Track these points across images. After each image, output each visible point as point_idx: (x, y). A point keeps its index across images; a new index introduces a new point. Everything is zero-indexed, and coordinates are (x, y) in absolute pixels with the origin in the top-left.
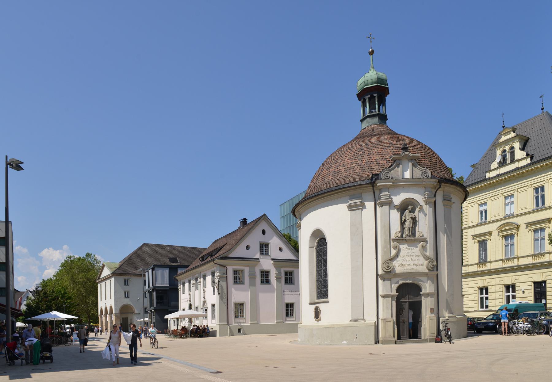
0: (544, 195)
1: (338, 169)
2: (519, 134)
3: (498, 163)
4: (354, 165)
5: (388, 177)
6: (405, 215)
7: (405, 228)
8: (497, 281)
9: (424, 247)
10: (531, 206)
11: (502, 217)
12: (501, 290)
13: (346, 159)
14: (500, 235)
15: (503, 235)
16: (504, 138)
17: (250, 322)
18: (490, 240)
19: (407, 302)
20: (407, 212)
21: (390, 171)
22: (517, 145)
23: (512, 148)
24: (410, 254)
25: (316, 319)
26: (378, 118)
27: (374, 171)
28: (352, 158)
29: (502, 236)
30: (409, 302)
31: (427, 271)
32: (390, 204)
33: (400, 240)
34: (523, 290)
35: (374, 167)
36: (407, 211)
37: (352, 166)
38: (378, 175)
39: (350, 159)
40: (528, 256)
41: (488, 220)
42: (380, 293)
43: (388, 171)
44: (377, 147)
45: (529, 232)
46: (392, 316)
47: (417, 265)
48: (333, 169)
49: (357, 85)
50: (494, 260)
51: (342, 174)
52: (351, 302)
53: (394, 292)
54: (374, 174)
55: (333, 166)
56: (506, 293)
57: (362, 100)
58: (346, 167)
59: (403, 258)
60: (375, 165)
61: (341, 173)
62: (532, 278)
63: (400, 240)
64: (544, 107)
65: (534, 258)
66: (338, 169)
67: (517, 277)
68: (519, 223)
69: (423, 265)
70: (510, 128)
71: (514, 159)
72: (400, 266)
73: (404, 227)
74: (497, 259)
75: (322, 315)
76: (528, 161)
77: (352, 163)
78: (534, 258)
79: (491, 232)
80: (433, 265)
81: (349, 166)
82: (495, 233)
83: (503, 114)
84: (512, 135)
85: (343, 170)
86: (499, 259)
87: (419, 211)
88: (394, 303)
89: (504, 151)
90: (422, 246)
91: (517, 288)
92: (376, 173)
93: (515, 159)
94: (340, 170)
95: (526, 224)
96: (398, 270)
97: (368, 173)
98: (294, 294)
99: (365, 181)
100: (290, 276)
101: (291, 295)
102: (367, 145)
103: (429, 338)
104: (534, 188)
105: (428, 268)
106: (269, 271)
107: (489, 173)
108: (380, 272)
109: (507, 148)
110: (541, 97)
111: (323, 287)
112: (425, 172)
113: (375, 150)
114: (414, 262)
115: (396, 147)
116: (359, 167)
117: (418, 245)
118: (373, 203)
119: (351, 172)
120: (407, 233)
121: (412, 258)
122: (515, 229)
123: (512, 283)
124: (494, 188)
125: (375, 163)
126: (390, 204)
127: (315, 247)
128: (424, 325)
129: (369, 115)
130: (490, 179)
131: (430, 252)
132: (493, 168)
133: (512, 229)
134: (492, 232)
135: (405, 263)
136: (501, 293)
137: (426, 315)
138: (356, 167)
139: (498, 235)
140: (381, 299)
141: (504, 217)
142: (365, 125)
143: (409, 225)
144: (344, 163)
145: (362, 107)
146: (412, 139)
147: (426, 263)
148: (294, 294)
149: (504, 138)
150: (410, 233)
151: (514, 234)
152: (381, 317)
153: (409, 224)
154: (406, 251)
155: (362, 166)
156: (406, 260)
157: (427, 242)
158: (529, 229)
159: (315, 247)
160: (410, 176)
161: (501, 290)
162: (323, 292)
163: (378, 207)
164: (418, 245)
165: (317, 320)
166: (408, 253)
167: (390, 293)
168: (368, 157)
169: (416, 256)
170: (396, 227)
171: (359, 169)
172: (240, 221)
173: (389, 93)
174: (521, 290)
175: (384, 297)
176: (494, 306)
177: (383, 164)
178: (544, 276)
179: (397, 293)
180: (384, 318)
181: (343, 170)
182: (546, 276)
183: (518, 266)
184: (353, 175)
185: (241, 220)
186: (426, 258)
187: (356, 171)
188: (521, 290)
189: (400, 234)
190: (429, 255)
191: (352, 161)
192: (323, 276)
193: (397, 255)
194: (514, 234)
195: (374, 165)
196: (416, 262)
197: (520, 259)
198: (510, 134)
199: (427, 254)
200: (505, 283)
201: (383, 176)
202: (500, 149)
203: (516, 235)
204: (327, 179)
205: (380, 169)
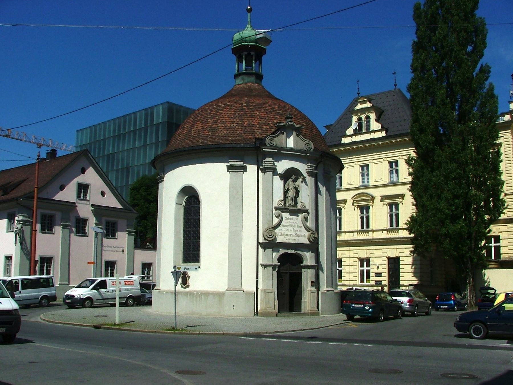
0: (398, 170)
1: (216, 126)
2: (375, 105)
3: (354, 130)
4: (235, 125)
5: (272, 143)
6: (289, 184)
7: (287, 197)
8: (351, 254)
9: (306, 219)
10: (387, 226)
11: (358, 186)
12: (355, 263)
13: (225, 117)
14: (355, 205)
15: (358, 205)
16: (359, 106)
17: (59, 283)
18: (345, 208)
19: (287, 273)
20: (290, 181)
21: (274, 138)
22: (373, 116)
23: (368, 118)
24: (292, 224)
25: (182, 285)
26: (254, 78)
27: (256, 135)
28: (233, 116)
29: (357, 206)
30: (290, 272)
31: (308, 243)
32: (274, 171)
33: (282, 209)
34: (377, 265)
35: (257, 131)
36: (290, 180)
37: (232, 125)
38: (261, 139)
39: (230, 117)
40: (382, 230)
41: (343, 187)
42: (261, 262)
43: (272, 138)
44: (259, 110)
45: (384, 205)
46: (273, 287)
47: (299, 236)
48: (210, 124)
49: (233, 39)
50: (348, 230)
51: (221, 132)
52: (228, 270)
53: (276, 262)
54: (257, 138)
55: (209, 120)
56: (361, 267)
57: (238, 55)
58: (226, 125)
59: (286, 228)
60: (258, 128)
61: (219, 130)
62: (386, 253)
63: (282, 209)
64: (396, 83)
65: (388, 232)
66: (216, 126)
67: (372, 251)
68: (374, 195)
69: (305, 236)
70: (366, 97)
71: (370, 129)
72: (282, 235)
73: (287, 196)
74: (351, 230)
75: (190, 282)
76: (384, 134)
77: (233, 122)
78: (388, 232)
79: (346, 201)
80: (315, 238)
81: (229, 125)
82: (350, 202)
83: (358, 81)
84: (368, 105)
85: (222, 128)
86: (354, 230)
87: (302, 182)
88: (275, 272)
89: (360, 119)
90: (305, 217)
91: (371, 263)
92: (260, 137)
93: (371, 129)
94: (219, 128)
95: (381, 196)
96: (280, 240)
97: (251, 136)
98: (116, 251)
99: (249, 144)
100: (50, 222)
101: (112, 251)
102: (248, 106)
103: (310, 311)
104: (388, 162)
105: (309, 239)
106: (87, 219)
107: (344, 138)
108: (261, 240)
109: (363, 116)
110: (394, 74)
111: (191, 250)
112: (308, 144)
113: (257, 113)
114: (296, 232)
115: (278, 114)
116: (240, 127)
117: (299, 215)
118: (255, 167)
119: (232, 132)
120: (290, 202)
121: (295, 228)
122: (370, 201)
123: (367, 257)
124: (350, 155)
125: (258, 126)
126: (274, 171)
127: (184, 204)
128: (305, 299)
129: (245, 72)
130: (345, 145)
131: (310, 224)
132: (349, 134)
133: (367, 200)
134: (347, 200)
135: (287, 233)
136: (355, 267)
137: (307, 287)
138: (237, 127)
139: (353, 205)
140: (260, 269)
141: (359, 187)
142: (239, 81)
143: (292, 195)
144: (223, 121)
145: (237, 62)
146: (292, 107)
147: (307, 234)
148: (116, 251)
149: (359, 106)
150: (293, 203)
151: (369, 205)
152: (260, 287)
153: (292, 193)
154: (289, 221)
155: (243, 128)
156: (288, 230)
157: (308, 213)
158: (384, 202)
159: (183, 205)
160: (294, 146)
161: (355, 263)
162: (191, 256)
163: (260, 171)
164: (299, 215)
165: (184, 286)
166: (291, 223)
167: (271, 263)
168: (250, 119)
169: (298, 227)
170: (278, 196)
171: (241, 130)
172: (47, 152)
173: (265, 54)
174: (376, 265)
175: (265, 266)
176: (348, 281)
177: (266, 129)
178: (398, 253)
179: (278, 263)
180: (266, 288)
181: (222, 128)
182: (400, 252)
183: (373, 239)
184: (234, 135)
185: (48, 151)
186: (307, 229)
187: (238, 132)
188: (376, 265)
189: (283, 203)
190: (310, 227)
191: (232, 120)
192: (192, 238)
193: (279, 225)
194: (369, 205)
195: (256, 128)
196: (298, 233)
197: (374, 232)
198: (366, 103)
199: (308, 224)
200: (360, 257)
201: (267, 141)
202: (356, 116)
203: (371, 207)
204: (202, 134)
205: (263, 133)
